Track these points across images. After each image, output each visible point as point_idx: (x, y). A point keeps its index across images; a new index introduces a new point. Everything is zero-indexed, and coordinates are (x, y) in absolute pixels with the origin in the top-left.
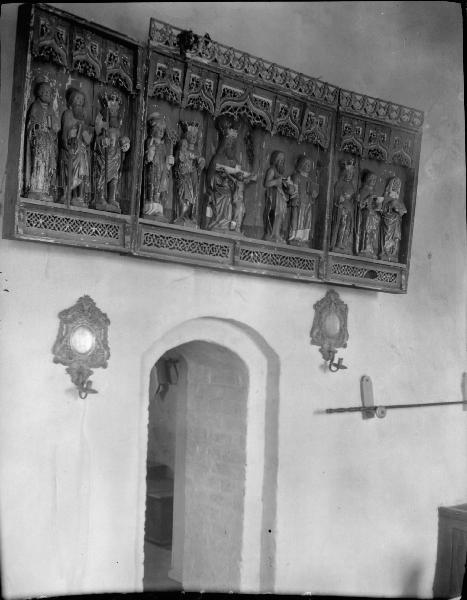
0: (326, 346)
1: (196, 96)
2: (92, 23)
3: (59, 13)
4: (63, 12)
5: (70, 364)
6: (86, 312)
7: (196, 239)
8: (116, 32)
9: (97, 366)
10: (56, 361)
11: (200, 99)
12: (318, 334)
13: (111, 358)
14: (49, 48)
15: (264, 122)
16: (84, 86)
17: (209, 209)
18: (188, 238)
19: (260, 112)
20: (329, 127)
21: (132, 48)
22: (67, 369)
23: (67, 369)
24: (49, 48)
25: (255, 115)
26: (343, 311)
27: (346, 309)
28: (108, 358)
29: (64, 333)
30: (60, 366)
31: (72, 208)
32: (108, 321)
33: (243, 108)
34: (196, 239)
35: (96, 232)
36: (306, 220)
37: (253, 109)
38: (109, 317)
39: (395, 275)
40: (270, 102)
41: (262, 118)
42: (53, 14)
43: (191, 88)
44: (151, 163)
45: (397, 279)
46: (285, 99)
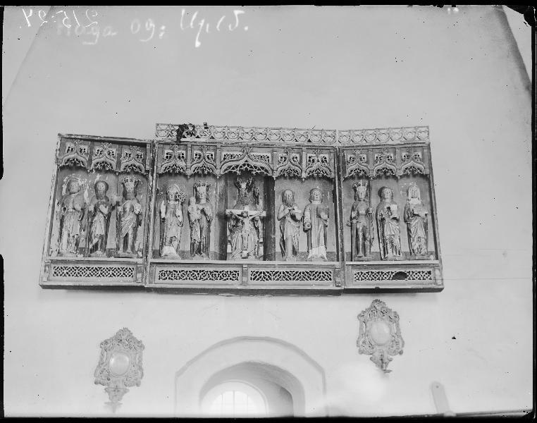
0: (377, 355)
1: (200, 165)
2: (105, 137)
3: (80, 137)
4: (82, 136)
5: (108, 384)
6: (124, 341)
7: (206, 269)
8: (132, 139)
9: (395, 353)
10: (361, 352)
11: (203, 166)
12: (364, 342)
13: (405, 345)
14: (74, 160)
15: (266, 171)
16: (110, 179)
17: (229, 246)
18: (198, 269)
19: (259, 164)
20: (333, 161)
21: (142, 145)
22: (105, 389)
23: (371, 359)
24: (74, 160)
25: (256, 167)
26: (394, 318)
27: (396, 316)
28: (403, 346)
29: (104, 359)
30: (100, 386)
31: (90, 259)
32: (142, 347)
33: (244, 165)
34: (206, 269)
35: (67, 273)
36: (319, 240)
37: (252, 163)
38: (143, 343)
39: (429, 273)
40: (269, 155)
41: (263, 168)
42: (75, 139)
43: (193, 160)
44: (164, 219)
45: (432, 276)
46: (283, 150)
